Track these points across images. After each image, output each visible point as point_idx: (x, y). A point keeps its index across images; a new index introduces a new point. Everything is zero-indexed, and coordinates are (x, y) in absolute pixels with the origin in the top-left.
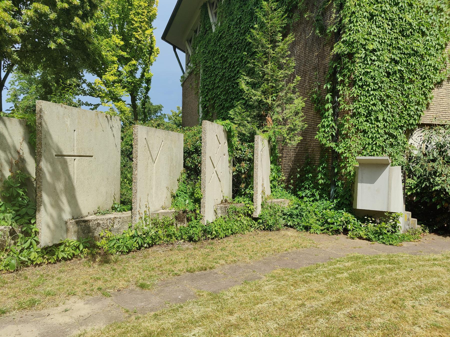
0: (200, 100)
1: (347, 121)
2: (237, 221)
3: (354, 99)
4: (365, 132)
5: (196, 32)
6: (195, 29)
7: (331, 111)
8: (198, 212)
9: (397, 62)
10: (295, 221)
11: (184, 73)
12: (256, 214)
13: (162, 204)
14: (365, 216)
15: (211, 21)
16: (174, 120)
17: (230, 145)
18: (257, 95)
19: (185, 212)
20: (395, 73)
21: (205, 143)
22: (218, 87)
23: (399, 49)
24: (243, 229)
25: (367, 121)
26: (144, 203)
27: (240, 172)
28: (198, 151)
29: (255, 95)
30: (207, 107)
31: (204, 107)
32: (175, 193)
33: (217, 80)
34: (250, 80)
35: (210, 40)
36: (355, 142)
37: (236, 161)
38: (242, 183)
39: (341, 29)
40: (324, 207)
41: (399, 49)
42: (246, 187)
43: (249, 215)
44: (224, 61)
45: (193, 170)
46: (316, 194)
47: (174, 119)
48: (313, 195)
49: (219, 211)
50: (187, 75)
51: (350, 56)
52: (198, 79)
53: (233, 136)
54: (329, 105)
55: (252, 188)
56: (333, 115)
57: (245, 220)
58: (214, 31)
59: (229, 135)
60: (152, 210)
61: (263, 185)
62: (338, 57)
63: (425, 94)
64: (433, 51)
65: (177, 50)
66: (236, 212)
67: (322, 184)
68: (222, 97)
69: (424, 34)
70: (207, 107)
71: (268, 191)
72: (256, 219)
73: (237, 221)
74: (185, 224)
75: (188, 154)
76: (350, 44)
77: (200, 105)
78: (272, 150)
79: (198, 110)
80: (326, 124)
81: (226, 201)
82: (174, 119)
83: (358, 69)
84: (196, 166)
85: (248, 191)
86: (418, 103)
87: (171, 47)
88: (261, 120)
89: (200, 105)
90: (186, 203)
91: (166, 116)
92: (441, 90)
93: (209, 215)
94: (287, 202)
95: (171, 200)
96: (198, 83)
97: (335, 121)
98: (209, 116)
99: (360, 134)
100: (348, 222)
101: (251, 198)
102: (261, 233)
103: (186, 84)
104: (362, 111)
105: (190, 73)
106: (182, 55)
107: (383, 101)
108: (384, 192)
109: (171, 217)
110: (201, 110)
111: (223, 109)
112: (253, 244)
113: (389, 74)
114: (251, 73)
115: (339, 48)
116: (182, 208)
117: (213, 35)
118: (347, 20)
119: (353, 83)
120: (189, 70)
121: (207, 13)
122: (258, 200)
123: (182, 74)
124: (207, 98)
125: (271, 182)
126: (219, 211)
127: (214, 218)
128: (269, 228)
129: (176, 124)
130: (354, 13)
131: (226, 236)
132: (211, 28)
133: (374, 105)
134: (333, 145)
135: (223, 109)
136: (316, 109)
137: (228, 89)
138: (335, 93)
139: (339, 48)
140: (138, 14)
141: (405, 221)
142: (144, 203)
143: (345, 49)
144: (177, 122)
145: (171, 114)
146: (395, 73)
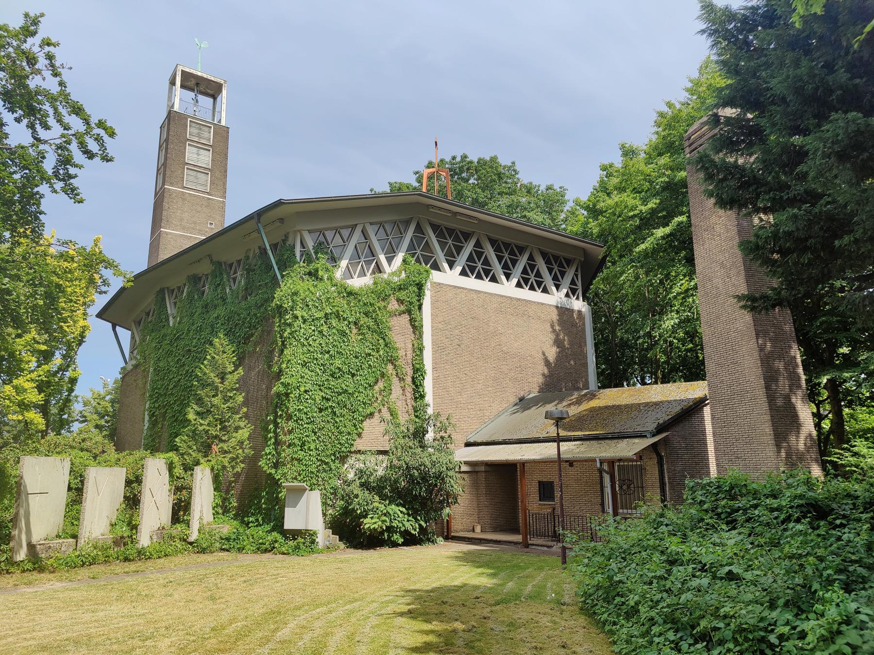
0: (147, 406)
1: (284, 450)
2: (171, 545)
3: (290, 432)
4: (299, 460)
5: (148, 314)
6: (147, 311)
7: (273, 440)
8: (134, 537)
9: (328, 400)
10: (230, 545)
11: (126, 362)
12: (192, 539)
13: (102, 531)
14: (295, 534)
15: (169, 312)
16: (94, 407)
17: (171, 475)
18: (203, 425)
19: (122, 537)
20: (326, 408)
21: (146, 477)
22: (172, 394)
23: (330, 388)
24: (177, 552)
25: (301, 450)
26: (88, 529)
27: (180, 500)
28: (138, 480)
29: (201, 425)
30: (156, 416)
31: (152, 415)
32: (113, 522)
33: (171, 387)
34: (199, 409)
35: (165, 336)
36: (289, 470)
37: (178, 489)
38: (180, 510)
39: (280, 373)
40: (261, 532)
41: (330, 388)
42: (184, 515)
43: (185, 540)
44: (181, 366)
45: (132, 501)
46: (260, 519)
47: (95, 404)
48: (257, 520)
49: (155, 537)
50: (130, 367)
51: (287, 395)
52: (146, 377)
53: (175, 468)
54: (272, 435)
55: (189, 514)
56: (274, 444)
57: (179, 544)
58: (171, 324)
59: (171, 467)
60: (94, 536)
61: (201, 511)
62: (278, 395)
63: (355, 426)
64: (361, 389)
65: (118, 328)
66: (172, 538)
67: (264, 509)
68: (176, 408)
69: (353, 375)
70: (156, 416)
71: (208, 517)
72: (191, 543)
73: (171, 545)
74: (123, 548)
75: (128, 483)
76: (286, 385)
77: (146, 413)
78: (216, 479)
79: (144, 419)
80: (268, 452)
81: (163, 528)
82: (95, 404)
83: (292, 407)
84: (135, 495)
85: (185, 518)
86: (349, 434)
87: (109, 325)
88: (206, 449)
89: (146, 413)
90: (125, 531)
91: (79, 399)
92: (372, 420)
93: (144, 540)
94: (228, 527)
95: (110, 528)
96: (146, 382)
97: (276, 449)
98: (154, 449)
99: (295, 462)
100: (276, 541)
101: (188, 524)
102: (195, 556)
103: (127, 378)
104: (296, 441)
105: (136, 367)
106: (125, 335)
107: (315, 433)
108: (308, 513)
109: (110, 542)
110: (147, 418)
111: (175, 421)
112: (184, 565)
113: (321, 410)
114: (200, 401)
115: (278, 388)
116: (120, 534)
117: (169, 331)
118: (284, 366)
119: (289, 417)
120: (134, 362)
121: (164, 299)
122: (195, 525)
123: (123, 364)
124: (157, 405)
125: (213, 509)
126: (155, 537)
127: (150, 543)
128: (203, 551)
129: (97, 413)
130: (289, 361)
131: (159, 557)
132: (167, 320)
133: (307, 436)
134: (273, 471)
135: (175, 421)
136: (260, 438)
137: (183, 400)
138: (276, 425)
139: (278, 388)
140: (71, 301)
141: (324, 536)
142: (88, 529)
143: (281, 389)
144: (99, 410)
145: (89, 396)
146: (326, 408)
